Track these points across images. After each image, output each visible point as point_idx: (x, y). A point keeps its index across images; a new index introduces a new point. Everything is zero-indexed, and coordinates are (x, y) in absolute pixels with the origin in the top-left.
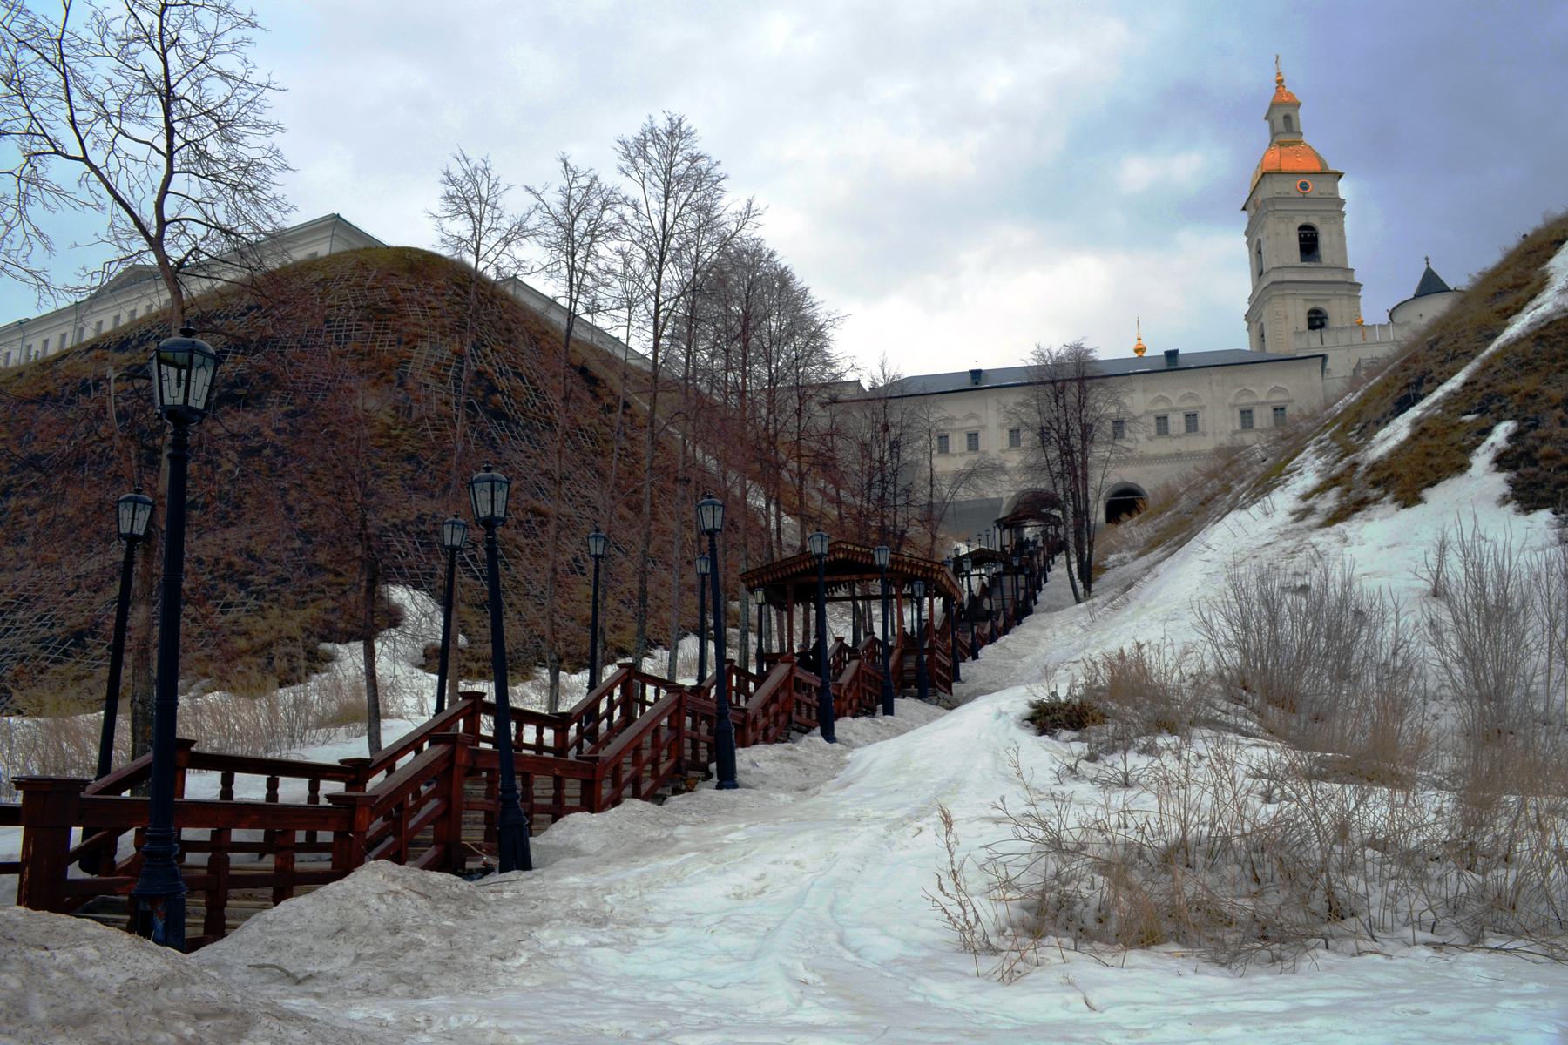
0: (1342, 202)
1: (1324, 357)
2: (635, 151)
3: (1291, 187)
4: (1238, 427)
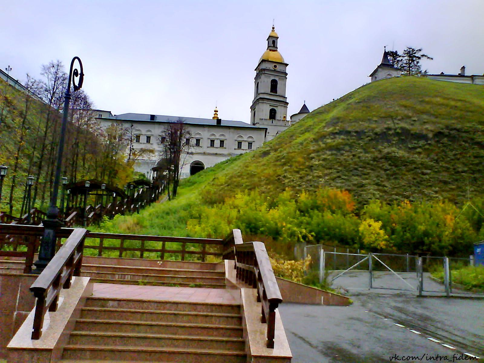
0: (286, 74)
1: (266, 129)
2: (46, 69)
3: (271, 66)
4: (237, 148)
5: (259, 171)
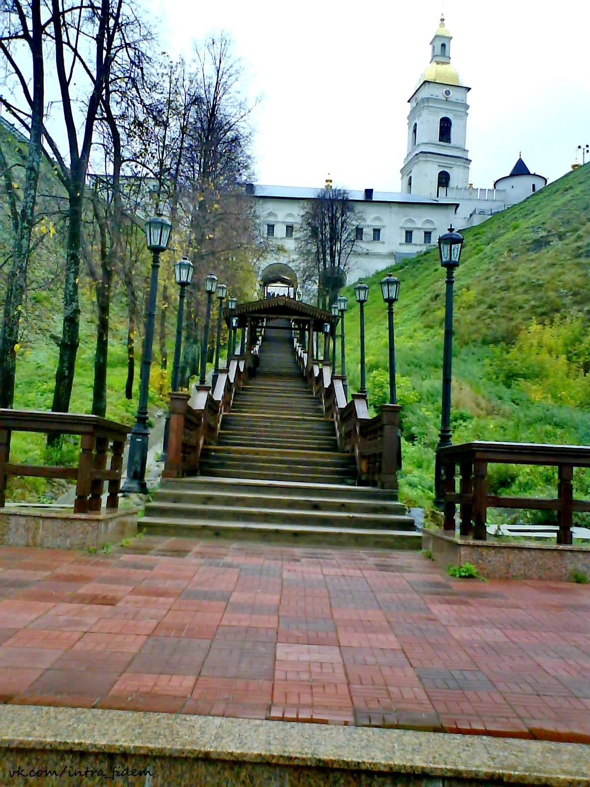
0: (467, 107)
3: (440, 92)
4: (404, 241)
5: (546, 277)
